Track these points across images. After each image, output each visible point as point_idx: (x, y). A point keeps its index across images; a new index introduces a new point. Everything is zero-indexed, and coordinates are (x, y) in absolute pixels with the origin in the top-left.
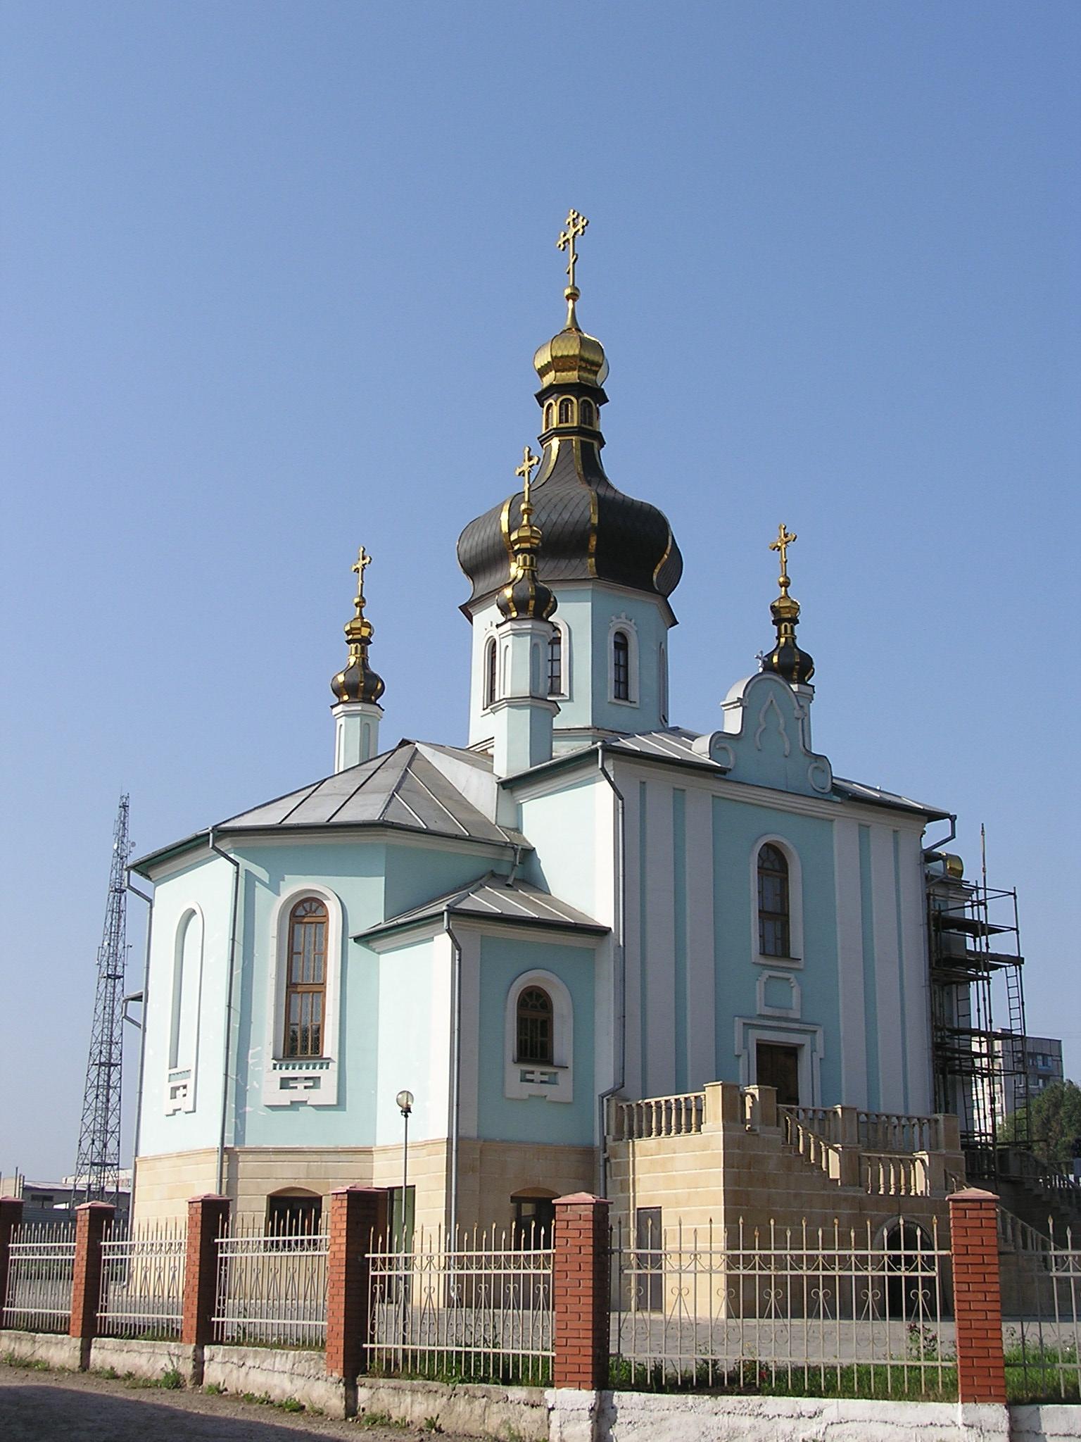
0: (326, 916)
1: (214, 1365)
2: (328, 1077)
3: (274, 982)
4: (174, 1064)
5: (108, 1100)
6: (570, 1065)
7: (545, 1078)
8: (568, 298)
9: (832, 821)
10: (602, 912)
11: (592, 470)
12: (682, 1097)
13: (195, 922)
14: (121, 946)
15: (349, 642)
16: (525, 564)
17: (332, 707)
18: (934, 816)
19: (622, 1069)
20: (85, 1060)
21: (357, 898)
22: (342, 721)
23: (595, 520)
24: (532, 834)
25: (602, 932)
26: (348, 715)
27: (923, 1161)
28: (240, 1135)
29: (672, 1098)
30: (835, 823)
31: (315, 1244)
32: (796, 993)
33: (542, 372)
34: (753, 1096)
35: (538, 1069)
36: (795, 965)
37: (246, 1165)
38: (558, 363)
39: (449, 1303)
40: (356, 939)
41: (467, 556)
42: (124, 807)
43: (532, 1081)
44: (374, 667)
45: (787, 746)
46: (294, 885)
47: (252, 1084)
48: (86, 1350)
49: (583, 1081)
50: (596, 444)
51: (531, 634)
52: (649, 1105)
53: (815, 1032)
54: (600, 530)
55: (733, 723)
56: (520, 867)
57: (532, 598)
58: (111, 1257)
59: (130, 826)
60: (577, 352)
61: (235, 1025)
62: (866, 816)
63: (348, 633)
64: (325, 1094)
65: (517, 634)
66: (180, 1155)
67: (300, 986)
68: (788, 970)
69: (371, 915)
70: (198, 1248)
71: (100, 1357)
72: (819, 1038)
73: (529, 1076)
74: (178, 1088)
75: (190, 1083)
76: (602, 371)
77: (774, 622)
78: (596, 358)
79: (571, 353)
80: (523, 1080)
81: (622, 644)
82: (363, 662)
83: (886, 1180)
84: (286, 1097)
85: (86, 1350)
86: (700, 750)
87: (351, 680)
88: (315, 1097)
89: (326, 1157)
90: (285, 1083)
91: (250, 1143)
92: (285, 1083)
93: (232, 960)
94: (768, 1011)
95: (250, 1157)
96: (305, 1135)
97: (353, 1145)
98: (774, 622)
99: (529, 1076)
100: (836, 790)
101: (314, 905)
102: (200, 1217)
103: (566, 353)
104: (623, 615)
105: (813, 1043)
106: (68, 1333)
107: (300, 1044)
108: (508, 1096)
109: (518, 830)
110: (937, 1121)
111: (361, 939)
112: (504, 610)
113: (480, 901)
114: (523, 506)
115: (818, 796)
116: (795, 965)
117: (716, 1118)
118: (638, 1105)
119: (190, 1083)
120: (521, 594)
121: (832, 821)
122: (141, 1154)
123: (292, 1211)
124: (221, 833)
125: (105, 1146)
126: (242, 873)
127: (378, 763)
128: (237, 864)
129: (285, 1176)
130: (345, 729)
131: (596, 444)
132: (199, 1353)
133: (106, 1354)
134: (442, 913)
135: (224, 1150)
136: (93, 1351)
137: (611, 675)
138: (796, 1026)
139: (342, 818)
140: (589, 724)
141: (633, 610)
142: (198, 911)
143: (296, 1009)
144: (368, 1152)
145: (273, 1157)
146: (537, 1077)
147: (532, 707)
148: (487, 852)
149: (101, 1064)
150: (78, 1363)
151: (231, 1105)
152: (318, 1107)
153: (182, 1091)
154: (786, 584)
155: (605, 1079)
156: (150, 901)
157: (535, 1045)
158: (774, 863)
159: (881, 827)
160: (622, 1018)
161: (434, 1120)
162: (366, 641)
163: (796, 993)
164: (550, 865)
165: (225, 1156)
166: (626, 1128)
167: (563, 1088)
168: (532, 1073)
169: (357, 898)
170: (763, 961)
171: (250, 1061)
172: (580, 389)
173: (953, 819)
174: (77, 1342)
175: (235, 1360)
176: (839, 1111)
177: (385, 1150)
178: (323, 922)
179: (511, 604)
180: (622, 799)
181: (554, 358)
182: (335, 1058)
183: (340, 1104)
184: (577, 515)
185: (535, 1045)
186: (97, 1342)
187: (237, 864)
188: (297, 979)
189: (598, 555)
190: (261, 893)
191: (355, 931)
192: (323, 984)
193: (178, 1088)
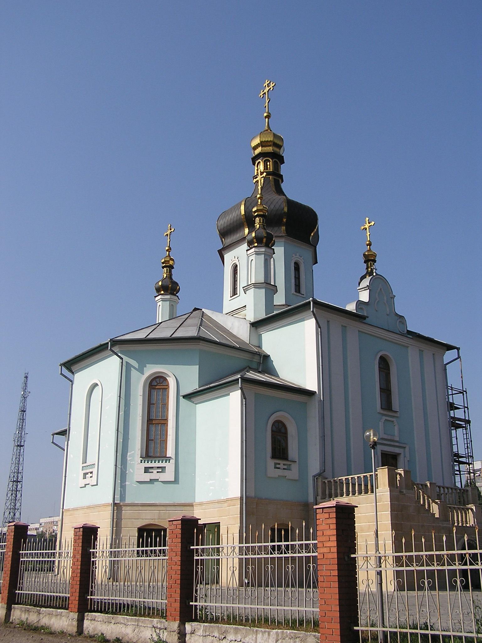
0: (168, 385)
1: (195, 638)
2: (170, 466)
3: (141, 418)
4: (85, 461)
5: (16, 496)
6: (297, 460)
7: (285, 467)
8: (266, 117)
9: (408, 347)
10: (311, 383)
11: (280, 191)
12: (350, 477)
13: (97, 390)
14: (23, 433)
15: (163, 267)
16: (260, 222)
17: (155, 297)
18: (450, 348)
19: (323, 462)
20: (7, 480)
21: (183, 376)
22: (160, 303)
23: (286, 209)
24: (267, 348)
25: (310, 394)
26: (163, 300)
27: (472, 509)
28: (123, 497)
29: (362, 475)
30: (409, 348)
31: (164, 552)
32: (396, 428)
33: (255, 148)
34: (400, 474)
35: (282, 462)
36: (395, 415)
37: (126, 512)
38: (262, 144)
39: (241, 584)
40: (184, 397)
41: (222, 227)
42: (26, 377)
43: (279, 468)
44: (174, 278)
45: (388, 310)
46: (151, 370)
47: (129, 470)
48: (81, 621)
49: (303, 470)
50: (280, 180)
51: (264, 254)
52: (341, 482)
53: (405, 448)
54: (288, 215)
55: (364, 296)
56: (263, 362)
57: (265, 237)
58: (26, 559)
59: (28, 385)
60: (272, 139)
61: (121, 440)
62: (423, 346)
63: (163, 263)
64: (169, 475)
65: (257, 254)
66: (89, 507)
67: (155, 422)
68: (394, 417)
69: (193, 385)
70: (179, 553)
71: (92, 626)
72: (407, 449)
73: (278, 466)
74: (87, 473)
75: (95, 471)
76: (282, 149)
77: (365, 262)
78: (280, 143)
79: (269, 140)
80: (276, 468)
81: (297, 267)
82: (170, 276)
83: (457, 518)
84: (147, 477)
85: (81, 621)
86: (351, 307)
87: (165, 284)
88: (163, 477)
89: (168, 508)
90: (147, 470)
91: (128, 500)
92: (147, 470)
93: (119, 407)
94: (385, 437)
95: (128, 508)
96: (157, 497)
97: (183, 501)
98: (365, 262)
99: (278, 466)
100: (409, 332)
101: (162, 380)
102: (180, 531)
103: (267, 140)
104: (298, 254)
105: (404, 452)
106: (67, 609)
107: (153, 449)
108: (269, 476)
109: (260, 347)
110: (467, 491)
111: (188, 397)
112: (250, 243)
113: (251, 375)
114: (258, 196)
115: (402, 335)
116: (395, 415)
117: (385, 486)
118: (334, 480)
119: (95, 471)
120: (260, 235)
121: (408, 347)
122: (64, 508)
123: (150, 535)
124: (115, 342)
125: (15, 515)
126: (124, 363)
127: (186, 316)
128: (122, 359)
129: (148, 518)
130: (162, 307)
131: (280, 180)
132: (182, 628)
133: (96, 624)
134: (238, 379)
135: (115, 504)
136: (85, 621)
137: (293, 281)
138: (397, 444)
139: (177, 335)
140: (284, 303)
141: (302, 253)
142: (99, 384)
143: (152, 433)
144: (191, 505)
145: (141, 508)
146: (281, 466)
147: (266, 288)
148: (246, 356)
149: (14, 481)
150: (75, 629)
151: (118, 481)
152: (164, 482)
153: (90, 475)
154: (370, 245)
155: (314, 467)
156: (71, 381)
157: (280, 451)
158: (384, 364)
159: (428, 351)
160: (323, 437)
161: (233, 487)
162: (171, 267)
163: (396, 428)
164: (277, 362)
165: (115, 507)
166: (327, 493)
167: (294, 473)
168: (279, 464)
169: (183, 376)
170: (382, 412)
171: (128, 459)
172: (273, 155)
173: (458, 349)
174: (75, 616)
175: (216, 634)
176: (429, 484)
177: (201, 504)
178: (166, 388)
179: (255, 240)
180: (320, 328)
181: (261, 142)
182: (174, 457)
183: (176, 481)
184: (277, 206)
185: (280, 451)
186: (88, 616)
187: (122, 359)
188: (153, 417)
189: (286, 225)
190: (134, 373)
191: (184, 392)
192: (167, 420)
193: (87, 473)
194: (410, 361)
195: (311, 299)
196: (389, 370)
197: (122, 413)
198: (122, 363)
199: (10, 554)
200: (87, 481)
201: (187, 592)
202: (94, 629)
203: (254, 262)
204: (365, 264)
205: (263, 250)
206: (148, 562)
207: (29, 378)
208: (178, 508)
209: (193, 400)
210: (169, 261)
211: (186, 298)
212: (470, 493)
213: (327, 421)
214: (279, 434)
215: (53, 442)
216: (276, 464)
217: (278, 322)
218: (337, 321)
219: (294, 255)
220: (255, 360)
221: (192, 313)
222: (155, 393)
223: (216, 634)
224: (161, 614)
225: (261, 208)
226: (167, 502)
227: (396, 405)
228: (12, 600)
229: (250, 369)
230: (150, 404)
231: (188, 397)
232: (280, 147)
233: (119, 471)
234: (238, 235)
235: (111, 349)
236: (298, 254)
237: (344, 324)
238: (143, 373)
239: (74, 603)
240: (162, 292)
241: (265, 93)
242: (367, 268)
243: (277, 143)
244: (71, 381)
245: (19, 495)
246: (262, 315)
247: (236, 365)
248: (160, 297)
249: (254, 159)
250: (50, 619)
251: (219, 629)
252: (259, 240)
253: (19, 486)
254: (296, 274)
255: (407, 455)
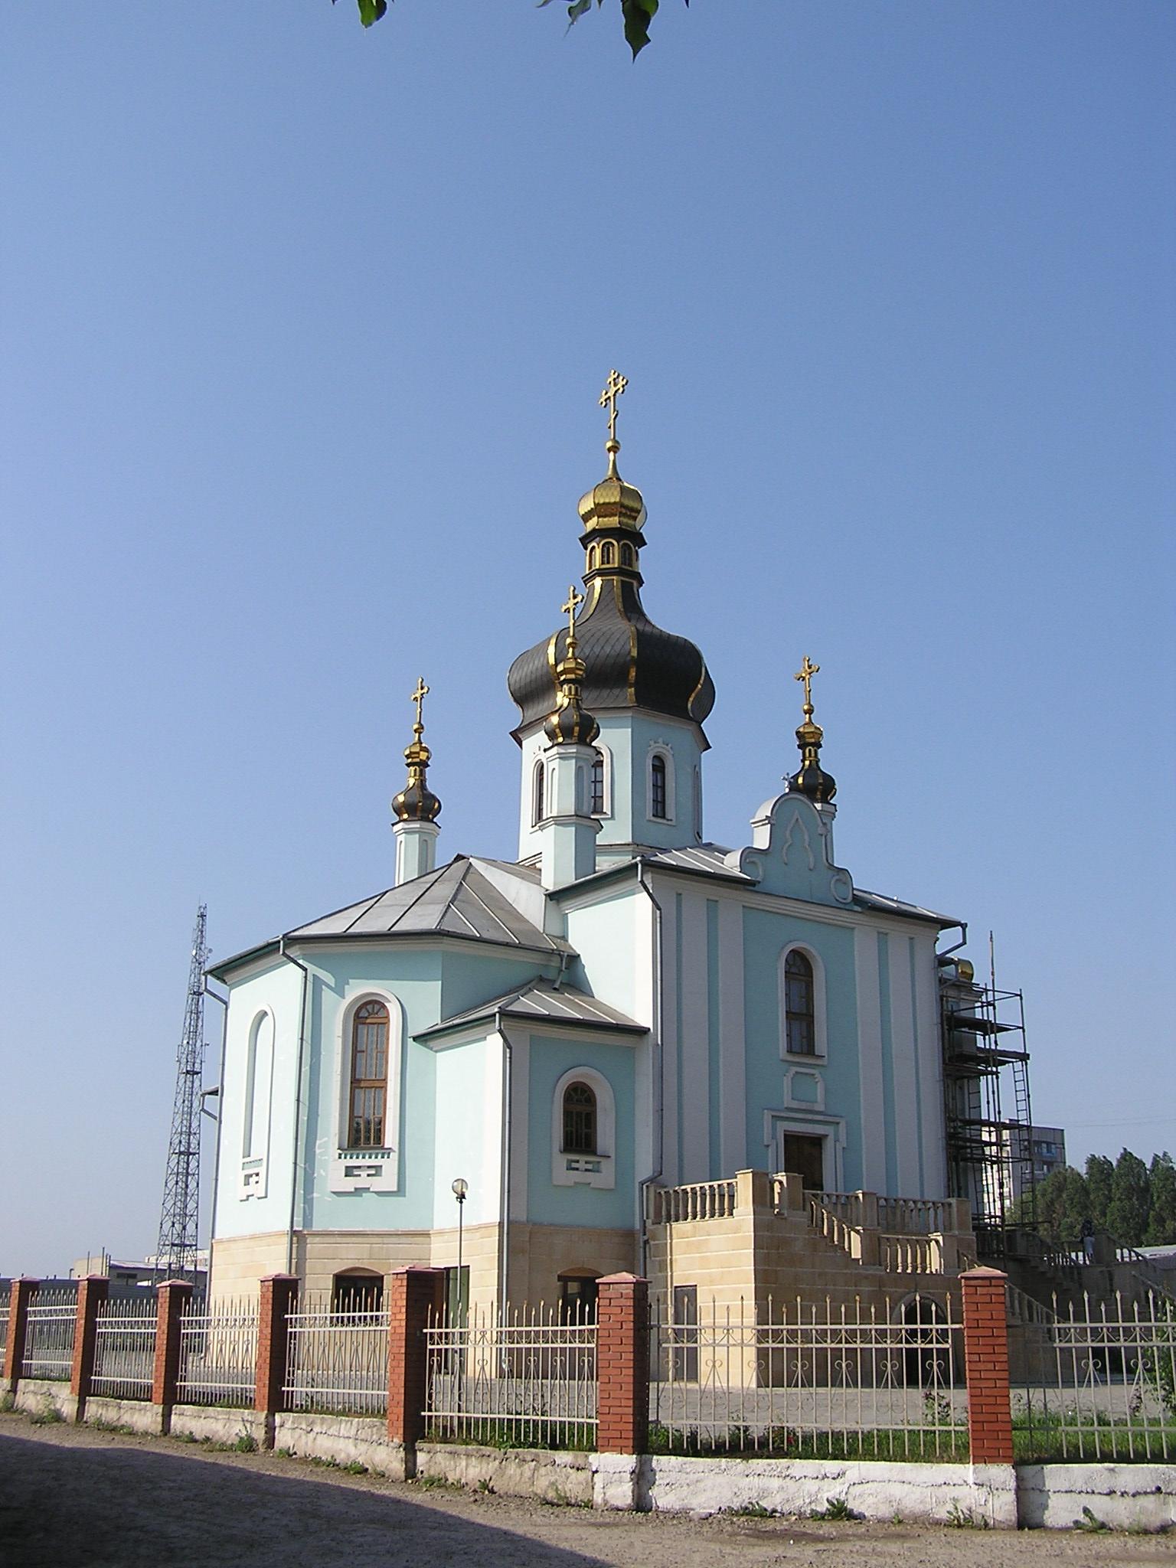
0: (387, 1017)
1: (284, 1431)
2: (390, 1165)
4: (247, 1153)
7: (590, 1167)
8: (609, 450)
10: (643, 1015)
11: (631, 607)
12: (715, 1184)
13: (267, 1022)
14: (199, 1044)
15: (408, 765)
19: (660, 1158)
21: (415, 1000)
23: (634, 653)
24: (577, 942)
25: (642, 1032)
26: (407, 832)
27: (937, 1242)
28: (308, 1220)
30: (856, 932)
33: (586, 518)
34: (781, 1183)
35: (583, 1158)
37: (313, 1246)
38: (600, 510)
40: (415, 1039)
42: (202, 916)
44: (431, 788)
46: (358, 989)
47: (319, 1172)
48: (167, 1416)
49: (624, 1170)
50: (635, 584)
52: (685, 1191)
55: (762, 839)
56: (564, 971)
57: (577, 724)
59: (207, 934)
61: (304, 1118)
63: (408, 757)
64: (388, 1181)
66: (253, 1237)
67: (364, 1083)
72: (842, 1127)
73: (574, 1165)
75: (262, 1171)
81: (659, 767)
82: (422, 784)
83: (903, 1259)
84: (350, 1184)
85: (167, 1416)
86: (731, 864)
89: (386, 1240)
90: (349, 1172)
91: (317, 1227)
92: (349, 1172)
94: (795, 1105)
95: (317, 1239)
99: (574, 1165)
101: (377, 1007)
107: (363, 1135)
110: (950, 1205)
111: (422, 1038)
112: (551, 735)
113: (528, 1004)
114: (569, 641)
116: (819, 1062)
120: (567, 721)
122: (217, 1236)
123: (356, 1289)
124: (290, 940)
125: (184, 1228)
126: (310, 978)
127: (435, 876)
128: (305, 970)
129: (352, 1257)
130: (405, 846)
131: (635, 584)
133: (185, 1419)
135: (294, 1233)
137: (650, 795)
140: (630, 840)
141: (669, 736)
145: (339, 1240)
146: (581, 1165)
150: (160, 1428)
151: (300, 1192)
154: (810, 712)
155: (645, 1168)
156: (225, 1003)
157: (580, 1137)
158: (799, 967)
159: (898, 933)
161: (487, 1205)
162: (424, 764)
167: (606, 1176)
169: (415, 1000)
170: (790, 1058)
172: (621, 533)
173: (964, 926)
174: (160, 1409)
175: (304, 1426)
177: (441, 1233)
178: (385, 1023)
181: (597, 505)
182: (396, 1148)
183: (400, 1191)
184: (618, 648)
185: (580, 1137)
187: (305, 970)
189: (636, 685)
190: (327, 995)
191: (419, 1027)
192: (385, 1080)
197: (306, 1069)
199: (83, 1322)
200: (249, 1190)
201: (173, 1368)
202: (183, 1426)
203: (556, 772)
206: (360, 1335)
207: (208, 919)
208: (403, 1239)
209: (431, 1044)
211: (453, 831)
212: (955, 1209)
213: (671, 1080)
214: (580, 1108)
216: (570, 1161)
218: (696, 895)
222: (363, 1030)
223: (304, 1426)
224: (247, 1402)
226: (385, 1229)
227: (821, 1044)
228: (19, 1372)
229: (524, 987)
230: (356, 1052)
231: (422, 1038)
232: (632, 513)
233: (300, 1173)
234: (540, 707)
238: (343, 997)
239: (158, 1393)
240: (405, 816)
243: (629, 506)
244: (225, 1003)
245: (192, 1185)
246: (570, 879)
247: (514, 981)
249: (585, 540)
250: (132, 1415)
251: (307, 1419)
252: (565, 730)
253: (193, 1164)
255: (843, 1137)
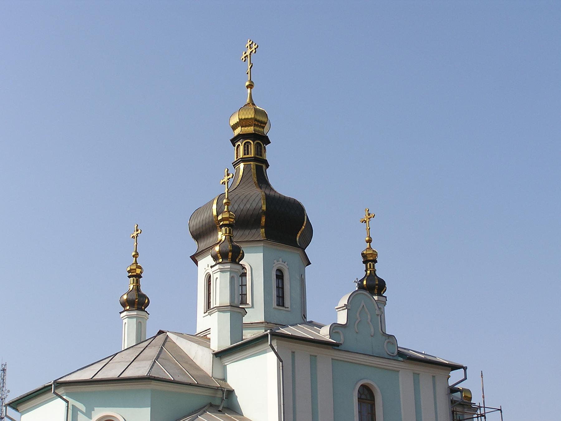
11: (262, 180)
15: (129, 277)
16: (226, 233)
17: (121, 313)
22: (126, 321)
23: (264, 208)
24: (232, 382)
26: (129, 317)
30: (400, 373)
33: (234, 127)
38: (242, 123)
44: (143, 290)
45: (372, 330)
50: (264, 166)
54: (267, 213)
55: (342, 318)
57: (230, 251)
60: (253, 116)
62: (419, 369)
76: (267, 126)
77: (364, 262)
79: (250, 117)
81: (280, 276)
82: (137, 288)
86: (324, 334)
104: (281, 260)
109: (224, 380)
112: (215, 258)
114: (225, 201)
120: (224, 249)
121: (398, 371)
124: (59, 384)
127: (146, 343)
128: (67, 402)
130: (128, 324)
131: (264, 166)
137: (274, 293)
139: (126, 375)
141: (286, 257)
147: (231, 312)
148: (207, 392)
159: (425, 373)
162: (139, 276)
172: (255, 137)
173: (465, 369)
180: (282, 361)
181: (241, 120)
184: (254, 205)
187: (67, 402)
189: (266, 227)
194: (401, 389)
195: (269, 331)
196: (374, 401)
198: (68, 407)
203: (218, 280)
204: (364, 265)
205: (228, 266)
210: (135, 269)
215: (465, 369)
217: (238, 354)
219: (275, 261)
220: (218, 396)
221: (155, 337)
225: (227, 216)
234: (212, 239)
235: (54, 393)
236: (281, 260)
237: (312, 354)
241: (247, 56)
242: (366, 271)
243: (260, 121)
246: (227, 344)
248: (125, 313)
254: (280, 286)
